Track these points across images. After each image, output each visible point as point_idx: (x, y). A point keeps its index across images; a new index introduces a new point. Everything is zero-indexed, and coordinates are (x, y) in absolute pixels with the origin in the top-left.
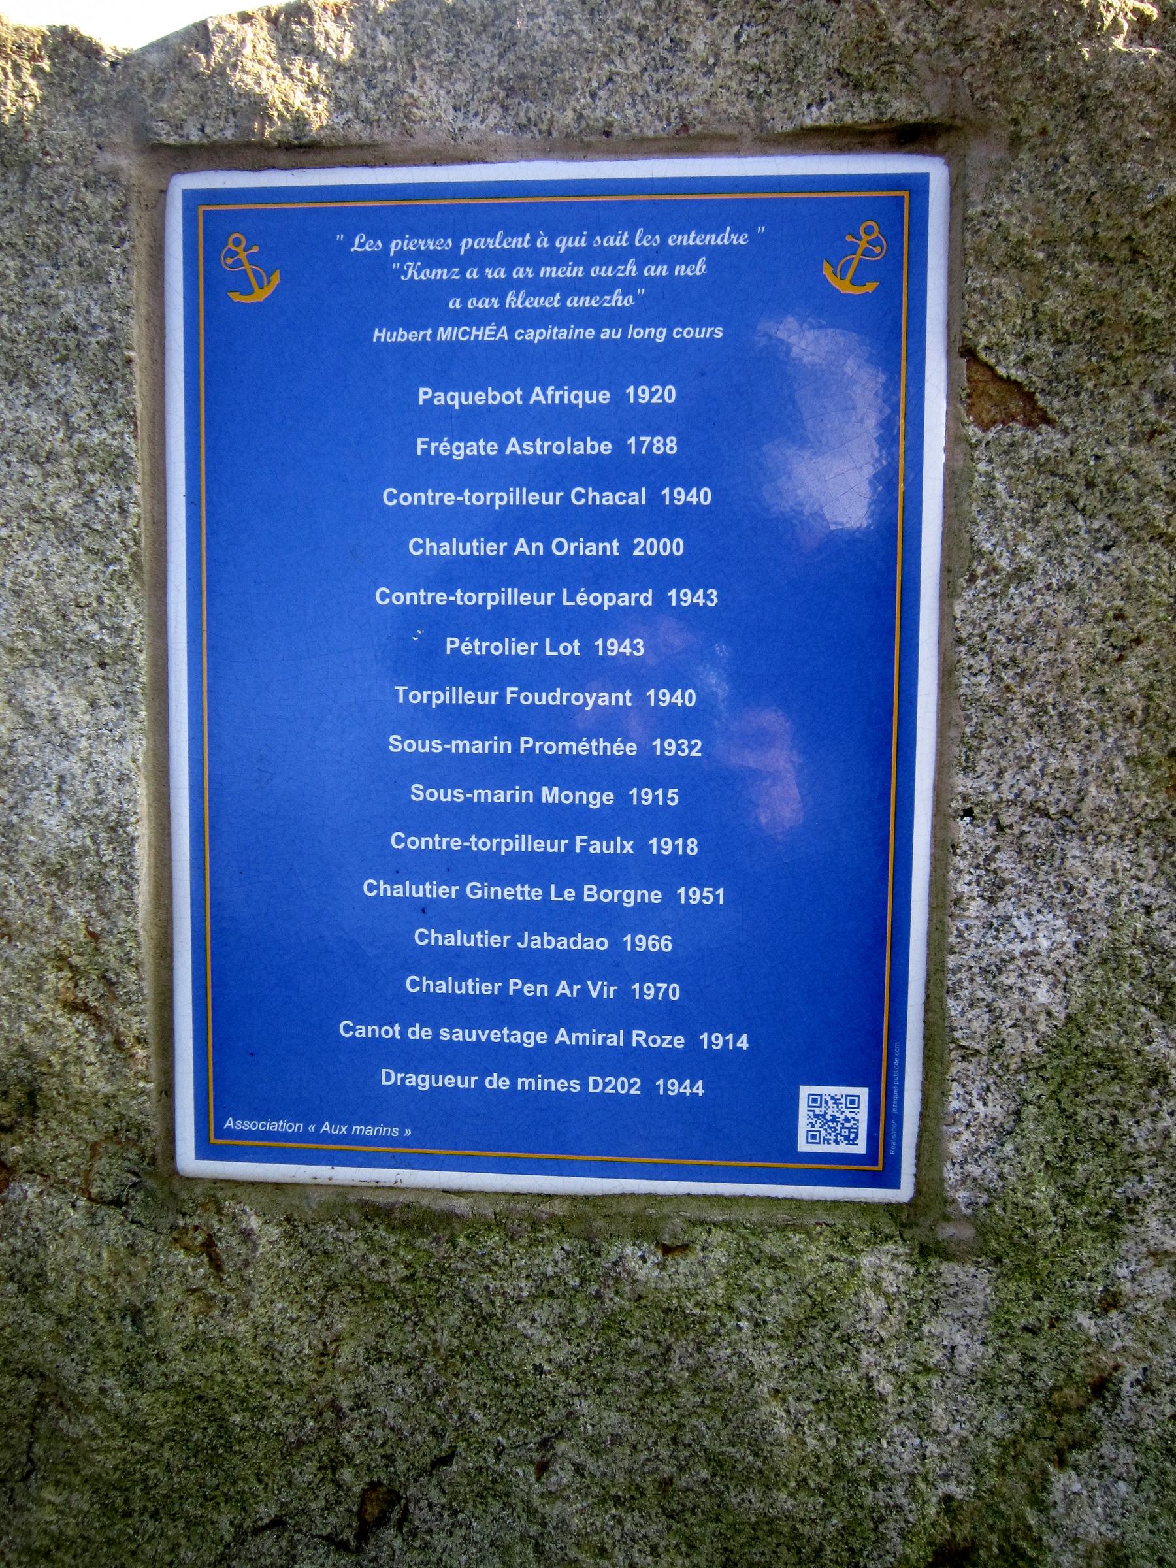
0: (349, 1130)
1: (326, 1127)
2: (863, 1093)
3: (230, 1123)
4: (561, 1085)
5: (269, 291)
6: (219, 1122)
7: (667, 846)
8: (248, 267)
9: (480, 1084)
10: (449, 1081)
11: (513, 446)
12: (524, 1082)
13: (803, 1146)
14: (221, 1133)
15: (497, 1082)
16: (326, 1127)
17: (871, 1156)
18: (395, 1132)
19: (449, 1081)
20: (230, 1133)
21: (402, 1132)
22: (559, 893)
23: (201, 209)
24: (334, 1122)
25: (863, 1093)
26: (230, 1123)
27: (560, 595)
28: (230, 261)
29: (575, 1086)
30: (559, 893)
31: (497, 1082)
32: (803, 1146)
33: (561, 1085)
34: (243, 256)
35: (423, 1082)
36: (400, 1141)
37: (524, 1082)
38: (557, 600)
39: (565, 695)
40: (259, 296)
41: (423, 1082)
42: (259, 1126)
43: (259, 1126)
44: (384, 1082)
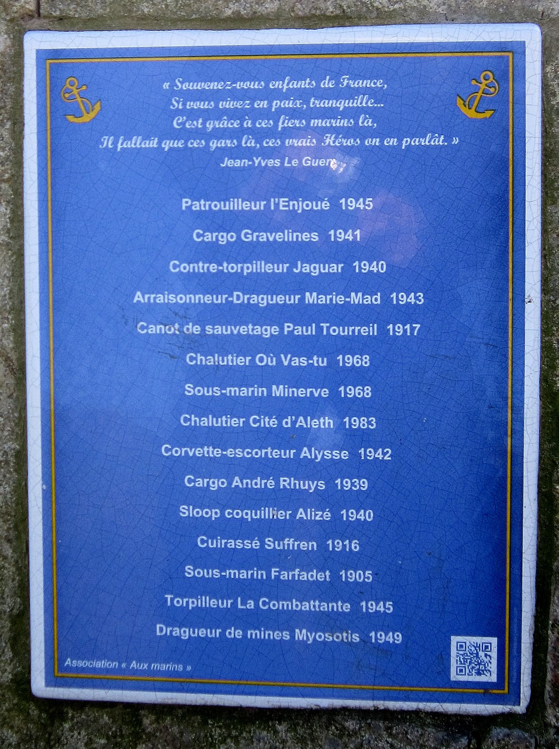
0: (149, 666)
1: (134, 665)
2: (494, 641)
3: (68, 662)
4: (276, 635)
5: (92, 115)
6: (61, 661)
7: (347, 484)
8: (79, 99)
9: (223, 634)
10: (202, 632)
11: (236, 482)
12: (252, 633)
13: (454, 676)
14: (61, 668)
15: (234, 633)
16: (134, 665)
17: (499, 684)
18: (180, 668)
19: (202, 632)
20: (69, 669)
21: (185, 668)
22: (244, 603)
23: (48, 61)
24: (139, 661)
25: (494, 641)
26: (68, 662)
27: (236, 602)
28: (67, 95)
29: (286, 636)
30: (244, 603)
31: (234, 633)
32: (454, 676)
33: (276, 635)
34: (75, 92)
35: (185, 633)
36: (184, 674)
37: (252, 633)
38: (234, 604)
39: (263, 482)
40: (87, 118)
41: (185, 633)
42: (88, 664)
43: (88, 664)
44: (158, 634)
